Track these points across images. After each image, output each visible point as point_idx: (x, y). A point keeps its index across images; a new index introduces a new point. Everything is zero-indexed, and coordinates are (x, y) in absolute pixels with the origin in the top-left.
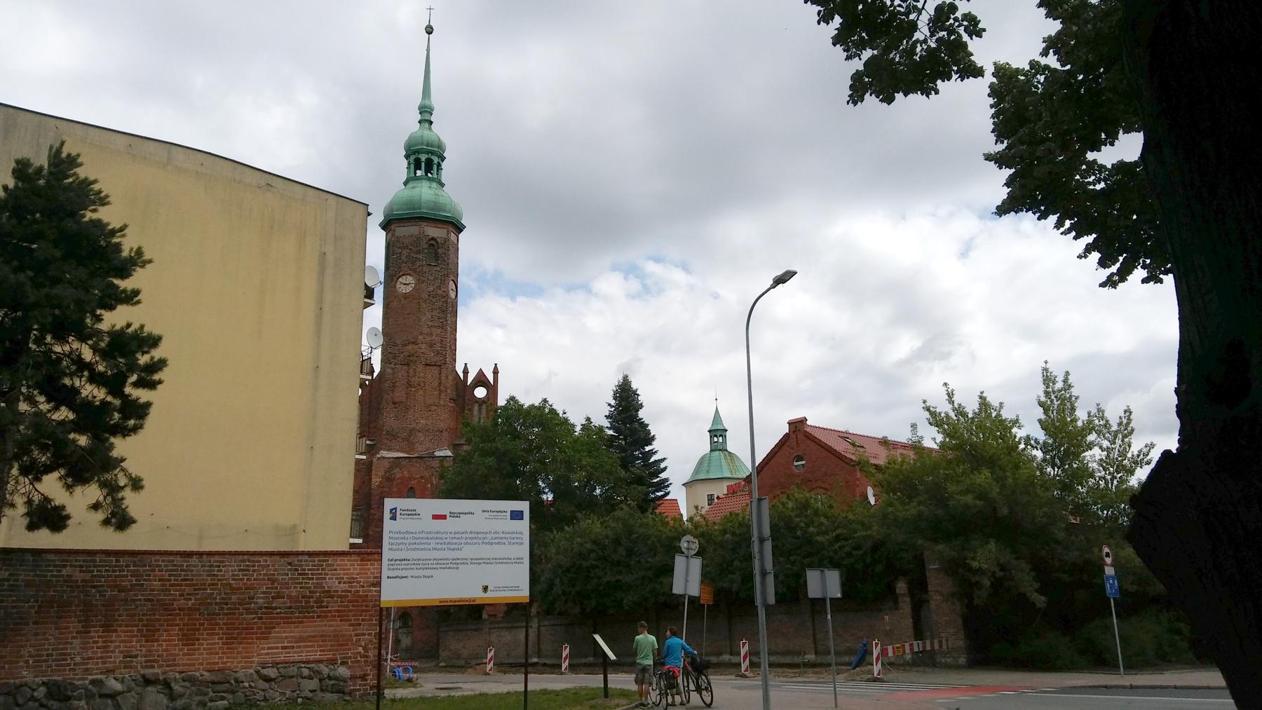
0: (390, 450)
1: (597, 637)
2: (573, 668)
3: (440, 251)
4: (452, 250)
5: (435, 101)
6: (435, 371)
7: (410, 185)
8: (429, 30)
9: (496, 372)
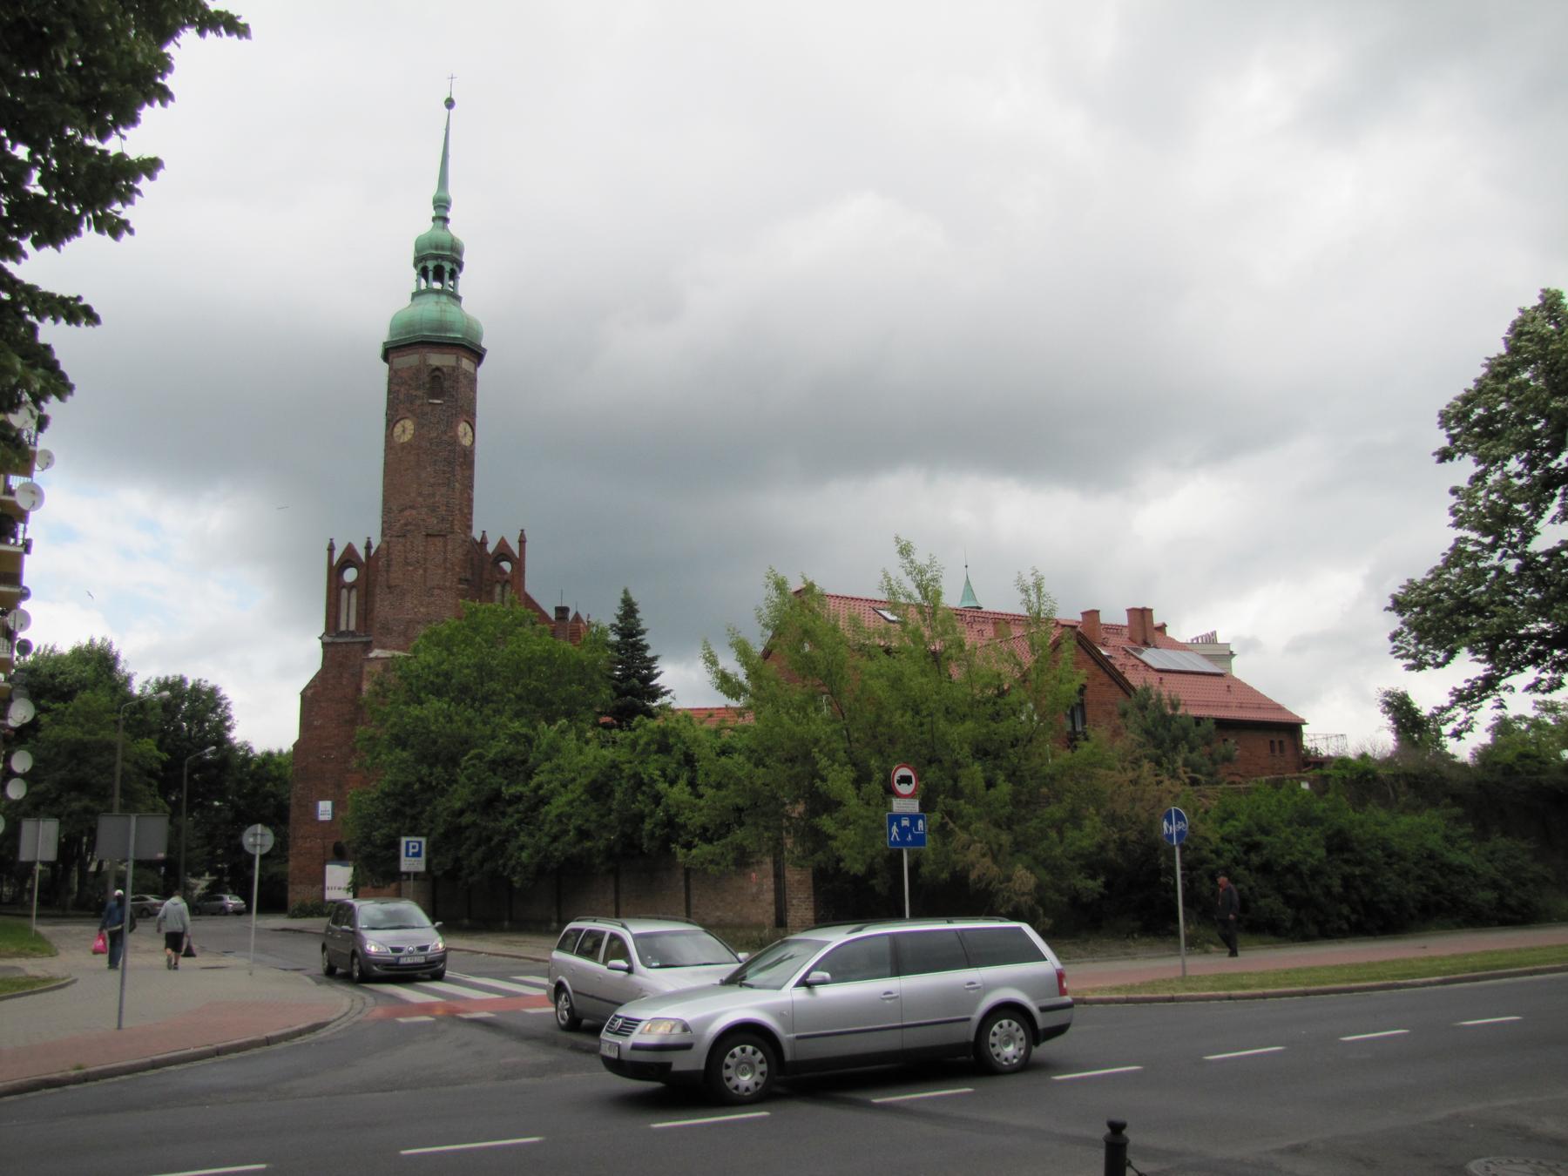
0: (384, 647)
1: (263, 1166)
2: (603, 933)
3: (447, 384)
4: (463, 381)
5: (453, 192)
6: (439, 542)
7: (417, 300)
8: (450, 103)
9: (522, 541)
